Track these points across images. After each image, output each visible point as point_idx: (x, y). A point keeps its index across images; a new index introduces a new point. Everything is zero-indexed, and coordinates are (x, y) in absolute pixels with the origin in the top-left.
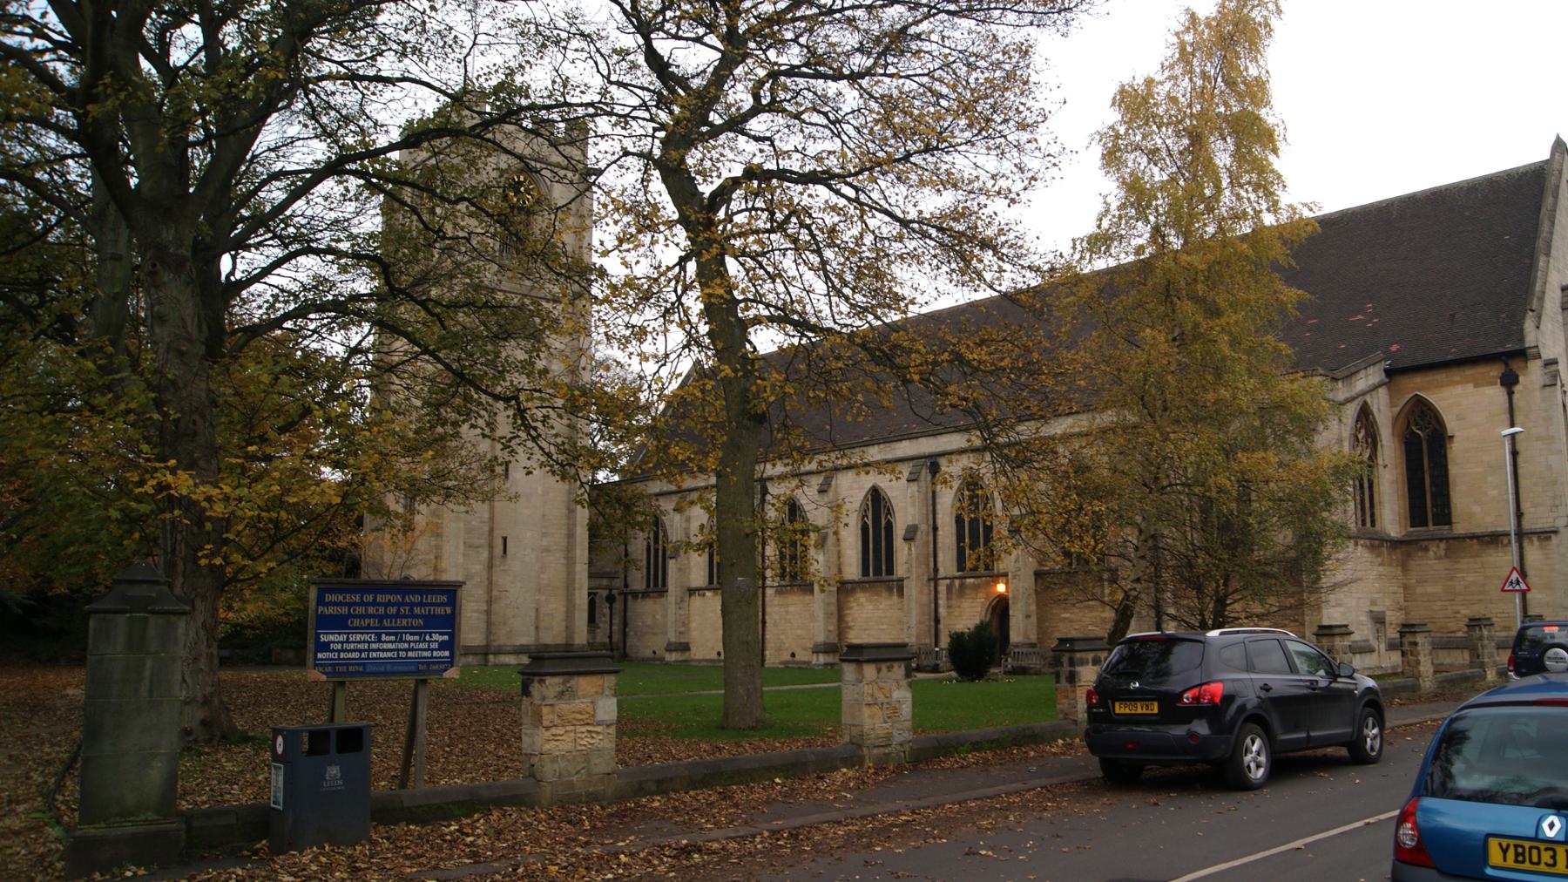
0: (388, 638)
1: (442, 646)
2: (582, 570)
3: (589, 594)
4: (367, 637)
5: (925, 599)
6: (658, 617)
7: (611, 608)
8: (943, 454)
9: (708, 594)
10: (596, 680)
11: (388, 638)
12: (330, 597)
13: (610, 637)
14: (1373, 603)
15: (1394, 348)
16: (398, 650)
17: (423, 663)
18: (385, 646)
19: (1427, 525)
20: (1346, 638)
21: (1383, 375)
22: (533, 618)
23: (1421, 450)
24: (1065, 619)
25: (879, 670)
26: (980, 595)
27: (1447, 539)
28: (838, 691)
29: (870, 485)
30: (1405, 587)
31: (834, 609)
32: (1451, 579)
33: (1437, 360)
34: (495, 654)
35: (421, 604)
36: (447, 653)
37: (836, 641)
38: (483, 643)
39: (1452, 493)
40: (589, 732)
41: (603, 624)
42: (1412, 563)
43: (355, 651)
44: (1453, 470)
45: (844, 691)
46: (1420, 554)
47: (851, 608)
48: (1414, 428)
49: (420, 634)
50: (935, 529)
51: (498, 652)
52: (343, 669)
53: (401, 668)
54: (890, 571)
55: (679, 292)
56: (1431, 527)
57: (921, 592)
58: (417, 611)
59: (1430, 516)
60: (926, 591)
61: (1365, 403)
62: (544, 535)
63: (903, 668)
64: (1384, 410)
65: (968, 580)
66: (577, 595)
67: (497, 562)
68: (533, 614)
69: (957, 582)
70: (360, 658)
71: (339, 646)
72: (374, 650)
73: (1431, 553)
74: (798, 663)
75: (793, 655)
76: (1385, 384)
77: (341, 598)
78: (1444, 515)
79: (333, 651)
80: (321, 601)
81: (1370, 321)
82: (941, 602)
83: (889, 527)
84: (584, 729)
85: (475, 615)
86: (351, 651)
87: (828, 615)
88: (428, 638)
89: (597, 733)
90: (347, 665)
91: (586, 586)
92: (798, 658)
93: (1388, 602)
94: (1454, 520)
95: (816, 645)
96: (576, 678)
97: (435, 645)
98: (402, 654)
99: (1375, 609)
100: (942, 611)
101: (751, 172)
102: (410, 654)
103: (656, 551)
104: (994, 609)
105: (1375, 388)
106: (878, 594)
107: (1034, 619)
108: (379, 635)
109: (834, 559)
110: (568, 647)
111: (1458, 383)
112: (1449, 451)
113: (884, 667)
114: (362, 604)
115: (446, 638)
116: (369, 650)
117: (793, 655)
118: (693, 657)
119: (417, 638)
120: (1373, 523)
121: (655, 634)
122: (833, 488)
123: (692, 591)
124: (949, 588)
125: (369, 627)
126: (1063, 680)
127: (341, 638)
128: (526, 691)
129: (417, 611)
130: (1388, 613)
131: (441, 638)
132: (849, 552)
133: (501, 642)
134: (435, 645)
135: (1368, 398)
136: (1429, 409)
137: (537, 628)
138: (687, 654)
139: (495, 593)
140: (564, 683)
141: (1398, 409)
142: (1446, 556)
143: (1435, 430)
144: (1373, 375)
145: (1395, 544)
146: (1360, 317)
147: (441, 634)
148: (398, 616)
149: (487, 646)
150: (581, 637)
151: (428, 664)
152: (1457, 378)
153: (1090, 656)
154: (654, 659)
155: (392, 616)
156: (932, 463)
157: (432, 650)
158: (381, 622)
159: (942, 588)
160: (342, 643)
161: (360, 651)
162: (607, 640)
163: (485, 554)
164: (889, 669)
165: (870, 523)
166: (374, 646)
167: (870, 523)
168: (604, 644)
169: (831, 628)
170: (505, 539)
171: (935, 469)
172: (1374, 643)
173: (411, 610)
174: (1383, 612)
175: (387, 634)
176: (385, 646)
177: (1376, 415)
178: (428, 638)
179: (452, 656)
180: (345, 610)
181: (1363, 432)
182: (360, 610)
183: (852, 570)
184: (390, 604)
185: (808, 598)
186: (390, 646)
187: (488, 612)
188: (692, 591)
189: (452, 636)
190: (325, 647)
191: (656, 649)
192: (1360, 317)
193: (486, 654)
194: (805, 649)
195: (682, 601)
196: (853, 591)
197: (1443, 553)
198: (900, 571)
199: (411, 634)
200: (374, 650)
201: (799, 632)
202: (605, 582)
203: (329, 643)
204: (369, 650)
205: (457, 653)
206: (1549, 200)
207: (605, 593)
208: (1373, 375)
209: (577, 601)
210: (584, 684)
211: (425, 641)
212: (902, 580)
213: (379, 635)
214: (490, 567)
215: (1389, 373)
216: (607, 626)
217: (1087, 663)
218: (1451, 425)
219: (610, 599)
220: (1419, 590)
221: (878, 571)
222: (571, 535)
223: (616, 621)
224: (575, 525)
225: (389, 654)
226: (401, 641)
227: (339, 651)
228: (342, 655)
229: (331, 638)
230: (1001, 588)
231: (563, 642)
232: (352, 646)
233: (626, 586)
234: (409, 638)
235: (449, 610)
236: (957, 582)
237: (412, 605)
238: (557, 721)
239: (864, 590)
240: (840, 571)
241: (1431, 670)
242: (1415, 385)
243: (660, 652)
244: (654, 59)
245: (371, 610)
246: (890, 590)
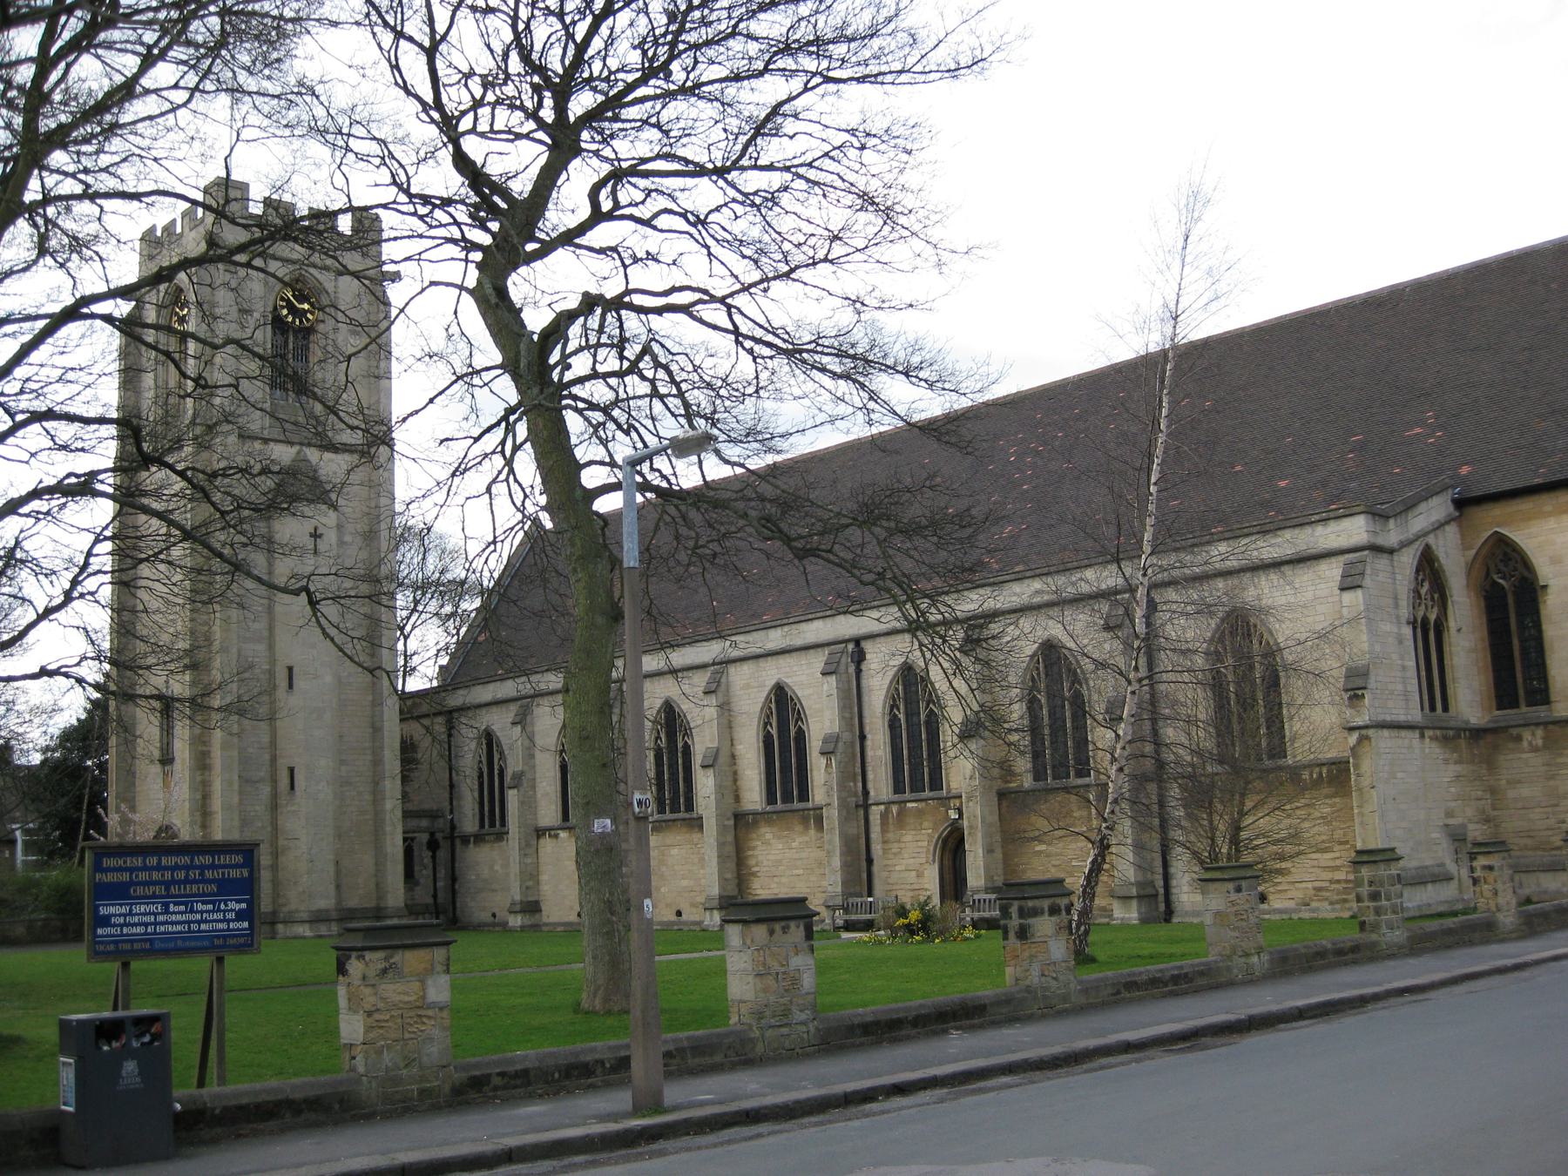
0: (176, 909)
1: (240, 916)
2: (392, 805)
3: (405, 840)
4: (152, 908)
6: (497, 867)
7: (434, 857)
8: (872, 637)
9: (563, 834)
10: (422, 954)
11: (176, 909)
12: (108, 862)
13: (435, 896)
14: (1449, 814)
15: (1465, 470)
16: (189, 922)
17: (218, 937)
18: (174, 918)
19: (1518, 707)
20: (1393, 864)
21: (1451, 508)
22: (332, 873)
23: (1506, 605)
24: (1041, 852)
25: (772, 932)
26: (926, 824)
27: (1546, 724)
28: (723, 959)
29: (773, 682)
30: (1493, 791)
31: (730, 849)
32: (1552, 777)
33: (1520, 485)
34: (285, 922)
35: (213, 867)
36: (246, 924)
37: (735, 893)
39: (1548, 662)
40: (420, 1016)
41: (423, 874)
42: (1502, 758)
43: (140, 924)
44: (1549, 631)
45: (729, 961)
46: (1511, 745)
47: (754, 848)
48: (1495, 577)
49: (213, 902)
50: (863, 737)
52: (127, 947)
53: (193, 944)
54: (804, 795)
55: (508, 453)
56: (1524, 709)
58: (209, 874)
59: (1521, 692)
61: (1427, 548)
62: (342, 762)
63: (802, 928)
64: (1453, 556)
65: (909, 805)
66: (388, 841)
67: (282, 801)
68: (332, 869)
69: (895, 809)
70: (146, 933)
71: (122, 920)
72: (163, 923)
73: (1525, 744)
74: (685, 923)
75: (679, 914)
76: (1453, 519)
77: (121, 862)
78: (1540, 694)
79: (115, 925)
80: (98, 867)
84: (412, 1014)
86: (135, 925)
87: (722, 858)
88: (222, 906)
89: (429, 1017)
90: (132, 941)
91: (400, 829)
92: (684, 917)
93: (1470, 812)
94: (1553, 698)
95: (709, 899)
96: (400, 952)
97: (232, 916)
98: (194, 927)
99: (1451, 821)
100: (877, 849)
101: (590, 302)
102: (203, 927)
104: (945, 841)
105: (1439, 526)
106: (788, 829)
107: (999, 855)
108: (166, 905)
109: (729, 783)
110: (378, 913)
111: (1550, 514)
112: (1542, 607)
113: (778, 927)
114: (145, 868)
115: (244, 906)
116: (156, 924)
117: (679, 914)
118: (545, 920)
119: (210, 907)
120: (1446, 709)
121: (494, 891)
122: (723, 687)
123: (540, 833)
125: (154, 896)
126: (1012, 935)
127: (123, 910)
128: (341, 969)
129: (209, 874)
130: (1471, 827)
131: (238, 907)
132: (748, 772)
133: (293, 907)
134: (232, 916)
135: (1431, 540)
136: (1514, 550)
137: (338, 887)
138: (537, 916)
139: (281, 842)
140: (386, 959)
141: (1473, 552)
142: (1545, 747)
143: (1524, 579)
145: (1477, 734)
146: (1418, 430)
147: (238, 901)
148: (187, 881)
150: (396, 895)
151: (225, 937)
152: (1548, 508)
153: (1046, 904)
154: (494, 925)
155: (179, 882)
156: (857, 649)
157: (228, 921)
158: (167, 889)
160: (125, 915)
161: (146, 925)
163: (266, 790)
164: (785, 930)
165: (774, 732)
166: (161, 918)
168: (427, 906)
169: (729, 876)
170: (292, 770)
171: (859, 657)
172: (1452, 867)
173: (202, 874)
174: (1464, 826)
175: (176, 904)
176: (174, 918)
177: (1443, 561)
178: (222, 906)
179: (251, 927)
180: (126, 877)
181: (1426, 586)
182: (143, 876)
183: (753, 795)
184: (176, 867)
185: (696, 836)
186: (179, 917)
188: (540, 833)
189: (250, 903)
190: (105, 921)
191: (496, 910)
192: (1418, 430)
193: (273, 923)
194: (693, 905)
195: (528, 845)
196: (755, 823)
197: (1540, 742)
198: (818, 795)
199: (204, 903)
200: (163, 923)
201: (685, 883)
202: (424, 823)
203: (110, 916)
204: (156, 924)
205: (257, 922)
207: (425, 837)
208: (1437, 508)
209: (389, 850)
210: (412, 960)
211: (219, 910)
213: (166, 905)
214: (274, 807)
215: (1461, 504)
217: (1042, 913)
218: (1545, 571)
219: (433, 845)
220: (1511, 794)
221: (787, 798)
222: (377, 762)
223: (442, 873)
224: (382, 748)
225: (179, 928)
226: (192, 911)
227: (121, 926)
228: (125, 930)
229: (112, 910)
231: (373, 904)
232: (136, 919)
234: (200, 907)
235: (246, 874)
236: (895, 809)
237: (202, 868)
238: (381, 1005)
239: (770, 822)
240: (737, 799)
241: (1514, 902)
242: (1492, 520)
243: (502, 915)
244: (462, 162)
245: (156, 876)
246: (805, 821)
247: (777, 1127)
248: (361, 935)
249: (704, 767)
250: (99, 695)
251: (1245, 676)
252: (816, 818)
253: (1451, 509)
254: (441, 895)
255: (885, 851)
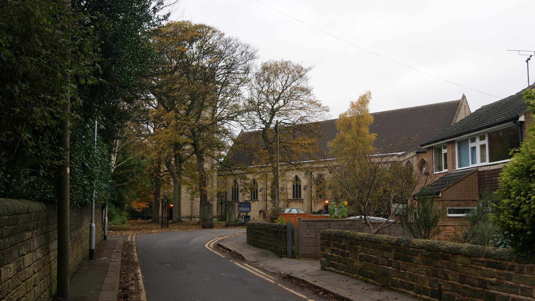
5: (308, 204)
7: (222, 206)
13: (221, 214)
34: (194, 218)
38: (190, 215)
51: (194, 218)
54: (300, 197)
57: (307, 202)
60: (309, 202)
69: (316, 200)
75: (254, 218)
81: (416, 139)
82: (312, 205)
83: (300, 186)
85: (188, 207)
92: (255, 219)
100: (313, 207)
103: (235, 189)
117: (254, 218)
124: (315, 201)
133: (195, 215)
144: (413, 154)
149: (191, 216)
159: (313, 202)
162: (221, 215)
167: (295, 185)
183: (290, 197)
187: (192, 207)
192: (414, 138)
193: (191, 218)
198: (303, 197)
206: (457, 112)
208: (413, 154)
212: (303, 199)
215: (417, 153)
216: (221, 211)
221: (297, 197)
230: (327, 202)
233: (226, 200)
236: (316, 200)
239: (293, 202)
246: (300, 202)
247: (301, 262)
248: (451, 227)
249: (260, 191)
250: (112, 172)
251: (235, 189)
252: (302, 201)
253: (416, 154)
254: (223, 214)
255: (315, 208)
